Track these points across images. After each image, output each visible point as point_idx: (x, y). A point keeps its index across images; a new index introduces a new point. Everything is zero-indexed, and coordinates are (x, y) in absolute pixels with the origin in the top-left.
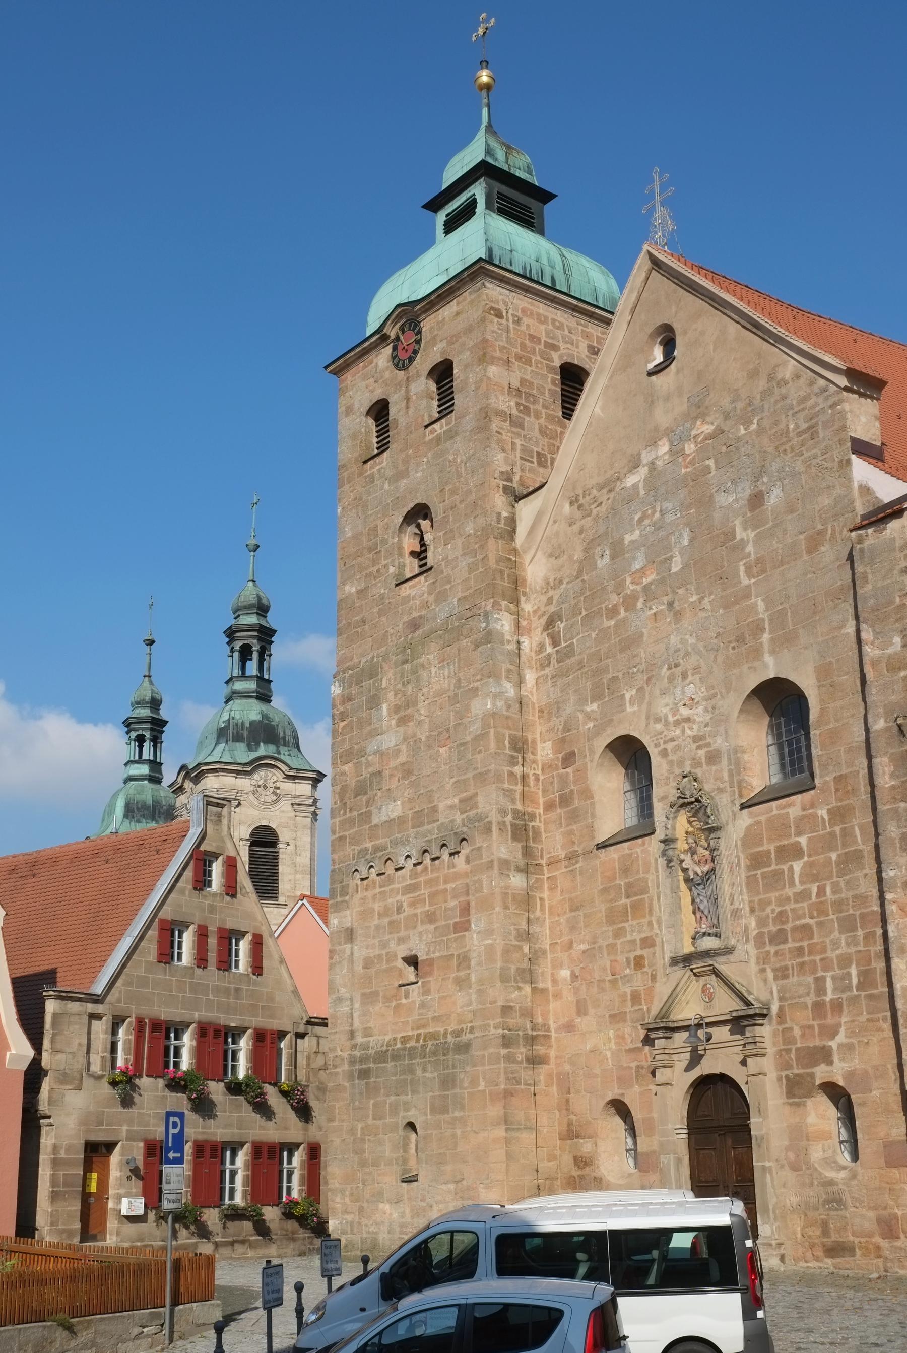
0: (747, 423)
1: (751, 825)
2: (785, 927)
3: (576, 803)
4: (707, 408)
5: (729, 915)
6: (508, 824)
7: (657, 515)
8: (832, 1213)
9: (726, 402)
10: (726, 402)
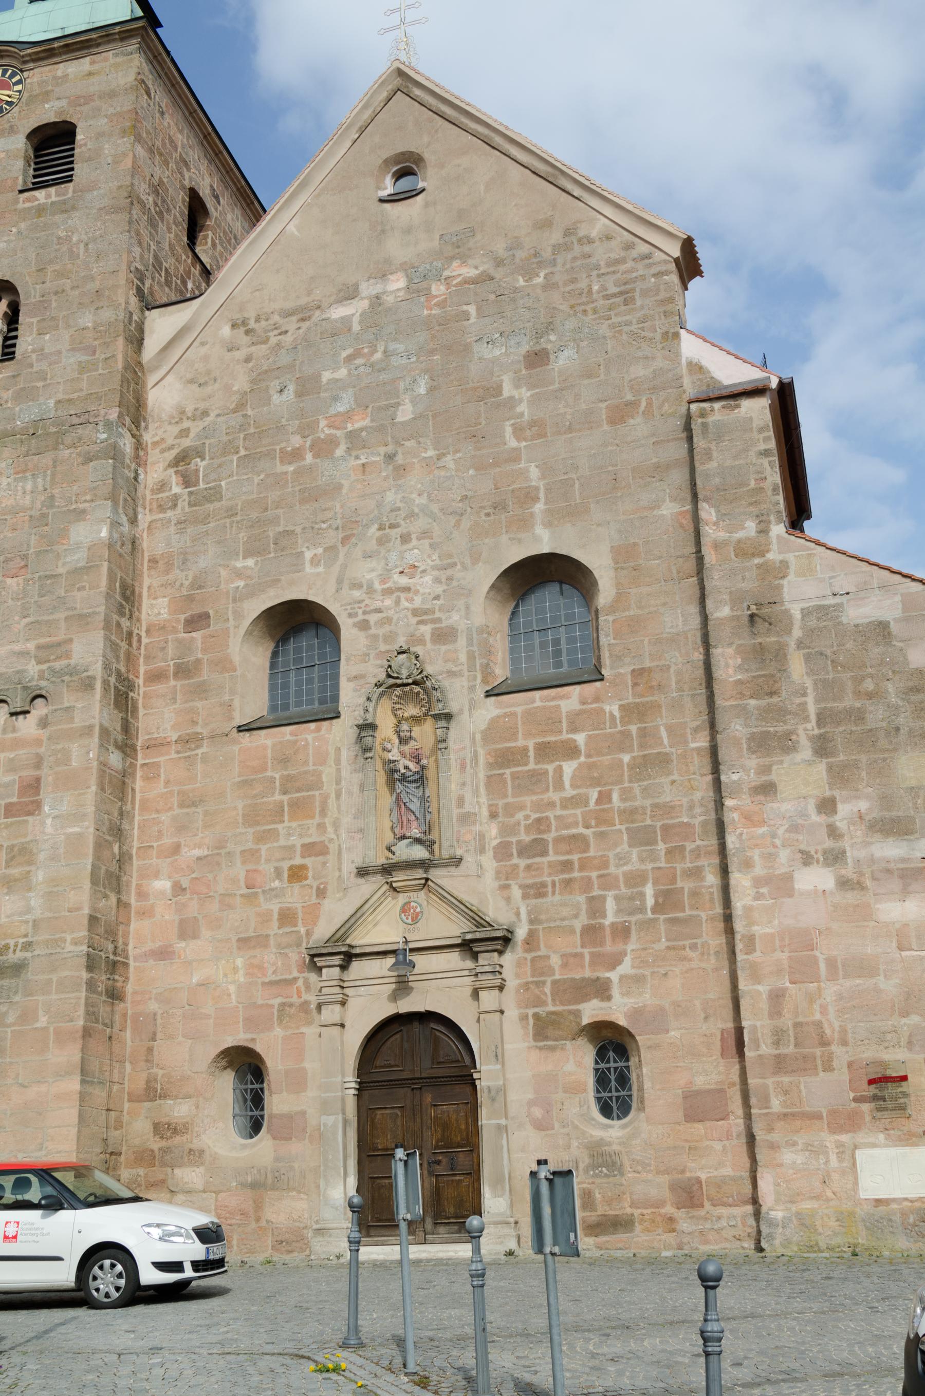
0: (529, 275)
1: (498, 717)
2: (545, 836)
3: (205, 674)
4: (470, 249)
5: (455, 820)
6: (112, 685)
7: (378, 355)
8: (598, 1181)
9: (500, 248)
10: (500, 248)
